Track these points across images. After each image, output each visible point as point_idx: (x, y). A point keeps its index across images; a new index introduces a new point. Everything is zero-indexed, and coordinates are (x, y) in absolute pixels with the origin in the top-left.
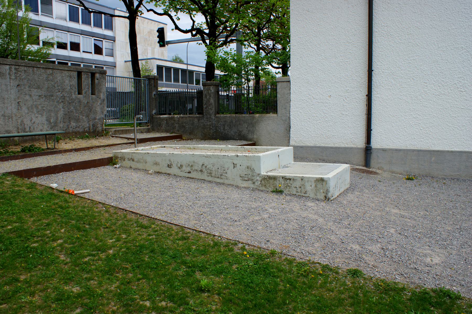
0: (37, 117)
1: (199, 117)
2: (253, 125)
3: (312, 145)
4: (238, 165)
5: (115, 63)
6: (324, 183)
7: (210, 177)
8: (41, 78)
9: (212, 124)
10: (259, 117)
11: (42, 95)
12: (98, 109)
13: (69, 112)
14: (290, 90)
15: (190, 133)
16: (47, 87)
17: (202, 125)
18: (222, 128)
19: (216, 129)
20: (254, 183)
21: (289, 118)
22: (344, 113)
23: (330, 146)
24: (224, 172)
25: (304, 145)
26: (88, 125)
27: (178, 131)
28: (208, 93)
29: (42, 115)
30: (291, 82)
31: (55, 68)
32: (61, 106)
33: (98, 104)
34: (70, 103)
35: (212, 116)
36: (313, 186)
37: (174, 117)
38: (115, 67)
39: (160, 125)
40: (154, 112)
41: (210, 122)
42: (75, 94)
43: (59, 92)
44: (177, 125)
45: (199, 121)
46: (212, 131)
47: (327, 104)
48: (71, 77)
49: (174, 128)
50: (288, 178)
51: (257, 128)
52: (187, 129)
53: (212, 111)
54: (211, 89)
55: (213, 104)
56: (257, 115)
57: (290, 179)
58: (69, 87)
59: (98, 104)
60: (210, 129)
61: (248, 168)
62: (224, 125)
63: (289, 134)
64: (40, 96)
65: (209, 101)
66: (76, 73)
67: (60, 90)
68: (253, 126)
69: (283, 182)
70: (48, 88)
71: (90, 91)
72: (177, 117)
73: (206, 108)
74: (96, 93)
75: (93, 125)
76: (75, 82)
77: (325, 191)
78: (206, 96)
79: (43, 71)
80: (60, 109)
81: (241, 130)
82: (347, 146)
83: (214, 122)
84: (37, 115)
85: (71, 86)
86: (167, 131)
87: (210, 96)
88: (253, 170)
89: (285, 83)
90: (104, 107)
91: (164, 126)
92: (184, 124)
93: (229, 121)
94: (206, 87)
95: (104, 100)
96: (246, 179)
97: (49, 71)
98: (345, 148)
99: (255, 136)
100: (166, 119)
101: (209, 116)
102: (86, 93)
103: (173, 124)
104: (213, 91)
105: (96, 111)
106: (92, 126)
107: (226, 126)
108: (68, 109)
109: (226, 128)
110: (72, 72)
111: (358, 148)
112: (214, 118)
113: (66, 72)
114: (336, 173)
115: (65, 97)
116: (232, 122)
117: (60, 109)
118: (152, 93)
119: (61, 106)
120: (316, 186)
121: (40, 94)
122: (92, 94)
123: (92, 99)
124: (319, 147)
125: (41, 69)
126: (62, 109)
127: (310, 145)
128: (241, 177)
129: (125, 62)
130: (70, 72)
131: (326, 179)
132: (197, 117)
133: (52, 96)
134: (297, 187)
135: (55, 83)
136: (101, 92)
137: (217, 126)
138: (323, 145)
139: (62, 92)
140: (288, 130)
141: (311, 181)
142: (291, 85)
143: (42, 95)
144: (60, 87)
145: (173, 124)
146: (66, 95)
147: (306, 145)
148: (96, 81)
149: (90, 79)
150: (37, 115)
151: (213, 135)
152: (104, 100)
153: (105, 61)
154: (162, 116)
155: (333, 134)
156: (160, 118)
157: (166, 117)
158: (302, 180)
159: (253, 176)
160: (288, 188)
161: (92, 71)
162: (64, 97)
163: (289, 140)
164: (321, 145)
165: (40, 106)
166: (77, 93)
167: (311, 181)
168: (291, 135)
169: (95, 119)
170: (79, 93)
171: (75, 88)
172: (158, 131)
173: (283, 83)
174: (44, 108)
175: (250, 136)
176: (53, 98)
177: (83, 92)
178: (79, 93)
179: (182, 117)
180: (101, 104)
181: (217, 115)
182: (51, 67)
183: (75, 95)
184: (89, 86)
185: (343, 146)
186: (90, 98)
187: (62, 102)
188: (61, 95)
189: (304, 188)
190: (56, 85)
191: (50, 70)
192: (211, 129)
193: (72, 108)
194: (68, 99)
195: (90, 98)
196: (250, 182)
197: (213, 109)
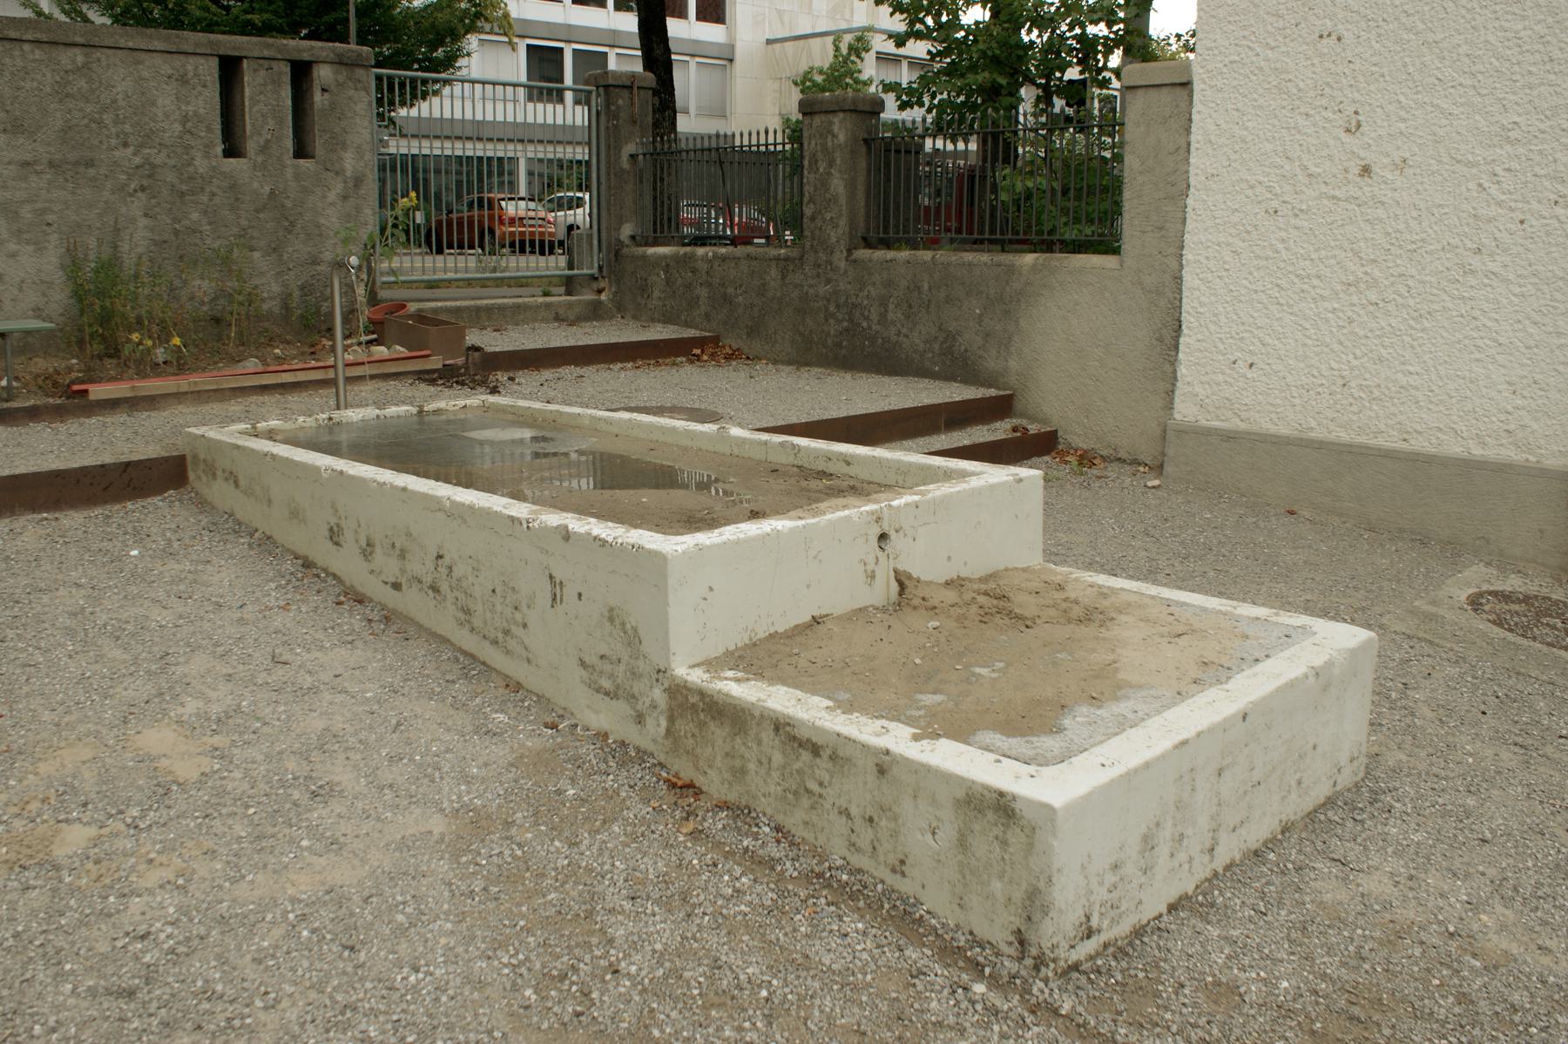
0: (13, 255)
1: (786, 259)
2: (1006, 302)
3: (1284, 431)
4: (570, 593)
5: (732, 47)
6: (1016, 838)
7: (465, 632)
8: (28, 85)
9: (836, 292)
10: (1034, 268)
11: (35, 162)
12: (332, 219)
13: (176, 233)
14: (1188, 131)
15: (752, 332)
16: (59, 123)
17: (795, 294)
18: (874, 317)
19: (851, 320)
20: (640, 719)
21: (1178, 279)
22: (1475, 262)
23: (1380, 442)
24: (518, 616)
25: (1243, 426)
26: (276, 288)
27: (707, 315)
28: (825, 148)
29: (40, 248)
30: (1197, 86)
31: (96, 41)
32: (136, 206)
33: (332, 196)
34: (182, 194)
35: (837, 255)
36: (948, 833)
37: (692, 256)
38: (731, 61)
39: (644, 289)
40: (627, 231)
41: (828, 281)
42: (207, 155)
43: (125, 145)
44: (703, 292)
45: (783, 278)
46: (833, 328)
47: (1380, 212)
48: (183, 80)
49: (693, 303)
50: (804, 734)
51: (1022, 323)
52: (741, 310)
53: (837, 234)
54: (836, 129)
55: (843, 200)
56: (1029, 258)
57: (816, 750)
58: (177, 127)
59: (332, 196)
60: (829, 316)
61: (611, 619)
62: (883, 302)
63: (1173, 362)
64: (26, 164)
65: (824, 184)
66: (215, 62)
67: (131, 139)
68: (1007, 312)
69: (778, 758)
70: (66, 129)
71: (289, 143)
72: (704, 258)
73: (813, 219)
74: (319, 150)
75: (302, 288)
76: (208, 101)
77: (1018, 895)
78: (814, 161)
79: (38, 54)
80: (133, 220)
81: (952, 326)
82: (1477, 452)
83: (842, 286)
84: (12, 247)
85: (185, 119)
86: (667, 319)
87: (831, 164)
88: (633, 638)
89: (1165, 95)
90: (358, 209)
91: (656, 294)
92: (730, 290)
93: (904, 283)
94: (817, 120)
95: (358, 182)
96: (606, 684)
97: (68, 57)
98: (1469, 467)
99: (1013, 364)
100: (666, 264)
101: (823, 257)
102: (264, 149)
103: (689, 286)
104: (842, 138)
105: (318, 226)
106: (297, 293)
107: (891, 307)
108: (176, 220)
109: (890, 316)
110: (192, 60)
111: (1544, 473)
112: (843, 265)
113: (158, 59)
114: (1166, 744)
115: (153, 166)
116: (918, 288)
117: (133, 220)
118: (618, 149)
119: (136, 206)
120: (962, 843)
121: (29, 157)
122: (301, 151)
123: (297, 177)
124: (1320, 445)
125: (26, 47)
126: (143, 222)
127: (1273, 429)
128: (583, 663)
129: (769, 42)
130: (178, 61)
131: (1027, 813)
132: (777, 259)
133: (90, 163)
134: (854, 811)
135: (105, 109)
136: (344, 147)
137: (855, 306)
138: (1344, 436)
139: (142, 146)
140: (1168, 340)
141: (933, 801)
142: (1197, 106)
143: (35, 162)
144: (127, 128)
145: (689, 286)
146: (159, 159)
147: (1255, 428)
148: (318, 97)
149: (286, 93)
150: (12, 247)
151: (839, 345)
152: (358, 182)
153: (614, 32)
154: (651, 251)
155: (1403, 380)
156: (644, 257)
157: (665, 257)
158: (881, 771)
159: (635, 674)
160: (806, 802)
161: (296, 56)
162: (151, 170)
163: (1170, 393)
164: (1332, 437)
165: (28, 207)
166: (219, 149)
167: (933, 801)
168: (1182, 371)
169: (315, 262)
170: (232, 151)
171: (209, 129)
172: (640, 314)
173: (1153, 93)
174: (50, 218)
175: (991, 363)
176: (92, 172)
177: (251, 146)
178: (232, 151)
179: (724, 259)
180: (345, 198)
181: (863, 253)
182: (79, 40)
183: (207, 157)
184: (281, 122)
185: (1455, 449)
186: (289, 173)
187: (143, 189)
188: (138, 160)
189: (895, 834)
190: (108, 118)
191: (77, 51)
192: (832, 315)
193: (195, 216)
194: (171, 177)
195: (289, 173)
196: (622, 706)
197: (843, 222)
